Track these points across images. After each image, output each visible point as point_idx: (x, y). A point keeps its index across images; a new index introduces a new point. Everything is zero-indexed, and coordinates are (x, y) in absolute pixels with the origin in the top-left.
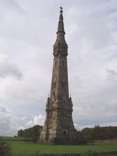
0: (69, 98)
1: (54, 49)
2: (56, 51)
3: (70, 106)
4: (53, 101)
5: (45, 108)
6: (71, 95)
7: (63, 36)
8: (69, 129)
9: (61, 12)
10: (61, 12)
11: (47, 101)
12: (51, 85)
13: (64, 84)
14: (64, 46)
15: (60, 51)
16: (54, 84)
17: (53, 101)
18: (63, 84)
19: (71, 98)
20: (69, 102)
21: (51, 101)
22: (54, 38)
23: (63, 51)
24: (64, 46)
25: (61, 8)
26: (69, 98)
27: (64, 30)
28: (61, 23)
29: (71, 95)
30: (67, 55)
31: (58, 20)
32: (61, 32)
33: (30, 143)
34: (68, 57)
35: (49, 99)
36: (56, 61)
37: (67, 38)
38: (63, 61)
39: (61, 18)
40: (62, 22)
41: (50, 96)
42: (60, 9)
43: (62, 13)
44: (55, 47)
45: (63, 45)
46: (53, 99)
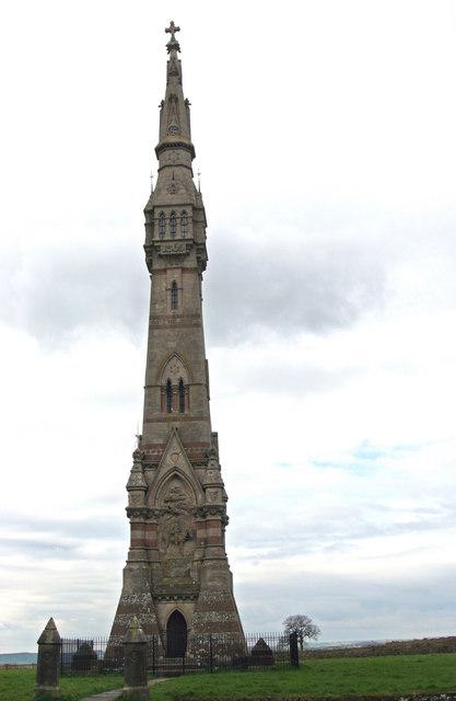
3: (146, 490)
9: (173, 47)
10: (173, 47)
15: (197, 244)
22: (144, 175)
36: (174, 284)
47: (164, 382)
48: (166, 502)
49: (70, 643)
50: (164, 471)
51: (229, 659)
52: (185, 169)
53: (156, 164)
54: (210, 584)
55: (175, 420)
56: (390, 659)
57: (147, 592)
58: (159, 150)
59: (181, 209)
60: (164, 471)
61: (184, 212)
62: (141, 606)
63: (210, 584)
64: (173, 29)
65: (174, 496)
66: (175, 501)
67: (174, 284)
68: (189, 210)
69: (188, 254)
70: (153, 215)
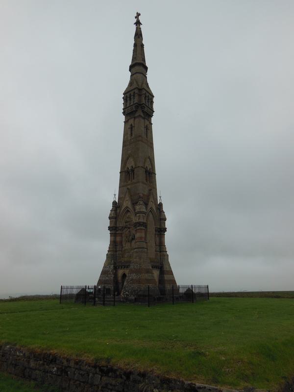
0: (158, 203)
3: (116, 218)
4: (127, 207)
5: (107, 223)
6: (160, 197)
7: (144, 75)
9: (138, 23)
10: (138, 23)
11: (110, 207)
12: (119, 175)
15: (141, 105)
17: (127, 207)
19: (161, 205)
22: (124, 79)
23: (147, 105)
28: (139, 48)
29: (160, 197)
32: (138, 66)
33: (67, 288)
34: (153, 120)
36: (132, 125)
37: (153, 80)
39: (138, 35)
40: (142, 46)
41: (117, 196)
43: (96, 285)
46: (127, 203)
47: (126, 169)
48: (126, 223)
49: (183, 287)
50: (149, 208)
51: (133, 298)
52: (142, 75)
53: (130, 74)
54: (135, 260)
55: (129, 185)
56: (277, 300)
57: (112, 265)
58: (131, 68)
59: (133, 91)
61: (134, 92)
63: (135, 260)
64: (138, 15)
65: (128, 220)
66: (129, 222)
67: (132, 125)
68: (136, 91)
69: (137, 110)
70: (128, 96)
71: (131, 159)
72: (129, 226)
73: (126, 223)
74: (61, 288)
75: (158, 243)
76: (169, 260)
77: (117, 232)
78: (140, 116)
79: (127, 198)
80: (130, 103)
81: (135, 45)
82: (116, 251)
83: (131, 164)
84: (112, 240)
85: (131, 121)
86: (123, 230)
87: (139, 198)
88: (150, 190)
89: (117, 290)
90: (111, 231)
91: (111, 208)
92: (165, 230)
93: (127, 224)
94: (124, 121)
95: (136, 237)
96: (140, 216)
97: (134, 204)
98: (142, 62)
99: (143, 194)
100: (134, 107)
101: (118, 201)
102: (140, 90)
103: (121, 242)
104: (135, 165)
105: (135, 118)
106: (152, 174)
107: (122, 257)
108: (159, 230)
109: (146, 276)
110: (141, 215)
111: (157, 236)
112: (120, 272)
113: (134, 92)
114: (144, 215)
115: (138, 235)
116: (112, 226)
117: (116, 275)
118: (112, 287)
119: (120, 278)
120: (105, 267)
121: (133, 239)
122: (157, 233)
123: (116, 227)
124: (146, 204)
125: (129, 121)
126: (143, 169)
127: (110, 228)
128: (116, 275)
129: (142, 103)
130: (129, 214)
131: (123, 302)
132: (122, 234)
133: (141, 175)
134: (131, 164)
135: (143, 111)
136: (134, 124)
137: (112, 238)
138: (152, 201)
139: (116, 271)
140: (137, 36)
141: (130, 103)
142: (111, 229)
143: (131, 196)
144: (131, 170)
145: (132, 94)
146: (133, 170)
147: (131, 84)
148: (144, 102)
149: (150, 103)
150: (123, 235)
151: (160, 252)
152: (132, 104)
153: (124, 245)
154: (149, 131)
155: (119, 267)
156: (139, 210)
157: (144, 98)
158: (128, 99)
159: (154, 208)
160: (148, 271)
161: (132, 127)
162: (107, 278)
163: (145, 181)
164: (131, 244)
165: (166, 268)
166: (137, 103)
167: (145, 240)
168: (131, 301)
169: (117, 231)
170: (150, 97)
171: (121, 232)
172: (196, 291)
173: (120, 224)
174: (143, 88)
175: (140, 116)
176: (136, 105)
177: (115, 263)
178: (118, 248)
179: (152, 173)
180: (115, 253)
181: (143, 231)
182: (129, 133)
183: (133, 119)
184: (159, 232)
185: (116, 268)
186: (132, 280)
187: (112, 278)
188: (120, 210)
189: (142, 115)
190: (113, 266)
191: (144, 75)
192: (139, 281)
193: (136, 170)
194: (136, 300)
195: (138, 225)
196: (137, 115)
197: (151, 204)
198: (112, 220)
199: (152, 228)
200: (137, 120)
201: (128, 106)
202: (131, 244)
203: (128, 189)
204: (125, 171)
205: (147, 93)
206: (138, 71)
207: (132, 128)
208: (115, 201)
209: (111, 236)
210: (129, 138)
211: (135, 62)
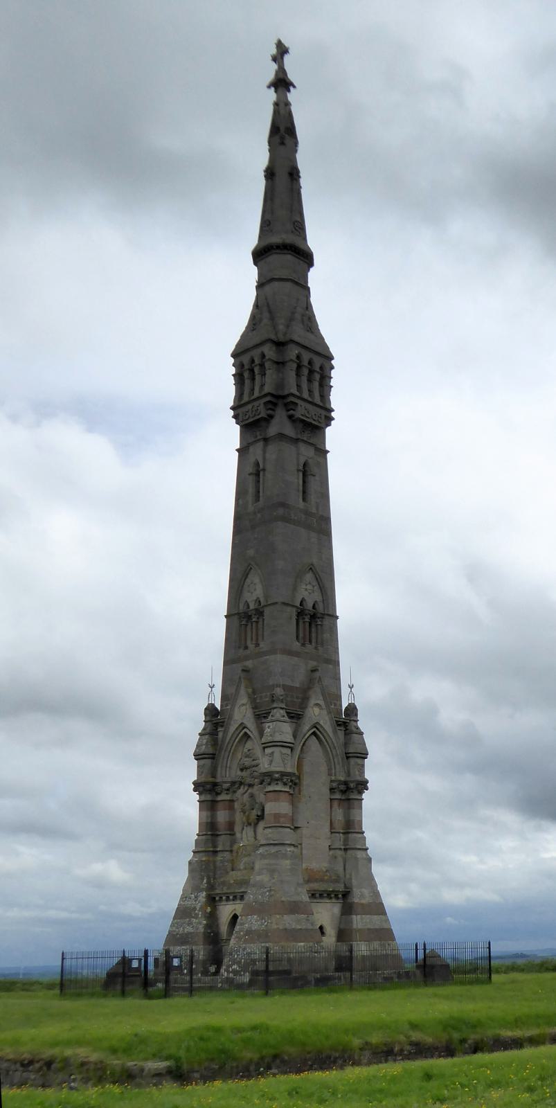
0: (345, 705)
1: (239, 378)
2: (256, 394)
4: (243, 726)
6: (351, 687)
7: (297, 283)
8: (346, 895)
9: (282, 83)
10: (282, 83)
11: (199, 723)
13: (313, 617)
14: (310, 363)
15: (284, 397)
16: (247, 616)
17: (243, 726)
18: (307, 619)
19: (352, 710)
20: (341, 734)
21: (232, 729)
23: (306, 395)
24: (310, 363)
25: (489, 943)
26: (345, 705)
27: (305, 239)
28: (282, 177)
29: (351, 687)
30: (329, 420)
31: (261, 157)
34: (333, 436)
35: (211, 711)
38: (305, 465)
40: (294, 174)
42: (272, 95)
44: (246, 359)
45: (306, 357)
46: (243, 714)
48: (242, 770)
50: (306, 727)
53: (253, 273)
57: (202, 891)
60: (232, 729)
62: (195, 909)
65: (247, 762)
68: (269, 351)
69: (271, 417)
71: (255, 579)
72: (248, 781)
73: (242, 770)
74: (63, 959)
75: (339, 827)
76: (373, 871)
77: (219, 798)
78: (281, 436)
79: (243, 699)
80: (262, 386)
81: (270, 174)
82: (215, 852)
83: (255, 592)
84: (204, 820)
85: (257, 451)
86: (235, 792)
87: (273, 701)
88: (314, 671)
89: (216, 959)
90: (200, 794)
91: (201, 725)
92: (363, 785)
93: (244, 774)
94: (238, 446)
95: (267, 812)
96: (273, 753)
97: (261, 716)
98: (290, 239)
99: (285, 687)
100: (262, 406)
101: (222, 706)
102: (280, 345)
103: (231, 826)
104: (266, 597)
105: (266, 440)
106: (323, 616)
107: (233, 870)
108: (343, 787)
109: (289, 921)
110: (277, 750)
111: (336, 804)
112: (226, 911)
113: (263, 356)
114: (288, 751)
115: (270, 808)
116: (203, 780)
117: (212, 917)
118: (202, 953)
119: (224, 928)
120: (183, 898)
121: (261, 817)
122: (338, 796)
123: (215, 784)
124: (295, 717)
125: (251, 449)
126: (289, 609)
127: (198, 786)
128: (212, 917)
129: (286, 392)
130: (249, 745)
131: (222, 989)
132: (232, 801)
133: (282, 626)
134: (255, 592)
135: (290, 417)
136: (264, 459)
137: (205, 813)
138: (317, 705)
139: (214, 908)
140: (277, 139)
141: (262, 386)
142: (201, 789)
143: (254, 692)
144: (256, 610)
145: (257, 361)
146: (260, 613)
147: (255, 322)
148: (294, 391)
149: (316, 384)
150: (236, 805)
151: (346, 850)
152: (256, 394)
153: (238, 835)
154: (313, 485)
155: (221, 898)
156: (270, 739)
157: (293, 374)
158: (246, 375)
159: (327, 725)
160: (294, 908)
161: (258, 472)
162: (189, 929)
163: (296, 645)
164: (255, 832)
165: (360, 896)
166: (269, 394)
167: (293, 820)
168: (240, 987)
169: (218, 794)
170: (318, 362)
171: (228, 797)
172: (446, 954)
173: (227, 773)
174: (292, 341)
175: (281, 436)
176: (268, 398)
177: (211, 887)
178: (222, 842)
179: (323, 616)
180: (211, 859)
181: (283, 796)
182: (251, 490)
183: (261, 444)
184: (343, 792)
185: (212, 900)
186: (249, 932)
187: (201, 929)
188: (225, 732)
189: (289, 430)
190: (205, 893)
191: (297, 283)
192: (263, 935)
193: (267, 611)
194: (251, 984)
195: (267, 780)
196: (273, 430)
197: (316, 713)
198: (203, 762)
199: (316, 786)
200: (272, 448)
201: (246, 399)
202: (255, 832)
203: (245, 671)
204: (238, 614)
205: (303, 352)
206: (277, 274)
207: (257, 474)
208: (213, 705)
209: (200, 810)
210: (251, 508)
211: (275, 239)
